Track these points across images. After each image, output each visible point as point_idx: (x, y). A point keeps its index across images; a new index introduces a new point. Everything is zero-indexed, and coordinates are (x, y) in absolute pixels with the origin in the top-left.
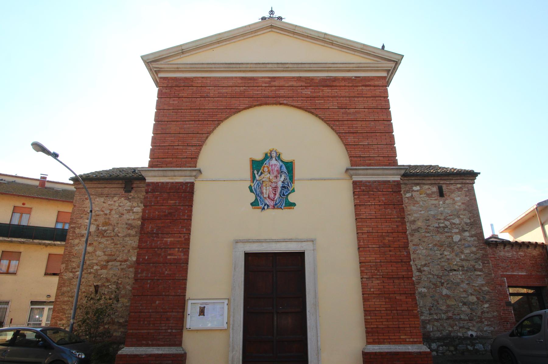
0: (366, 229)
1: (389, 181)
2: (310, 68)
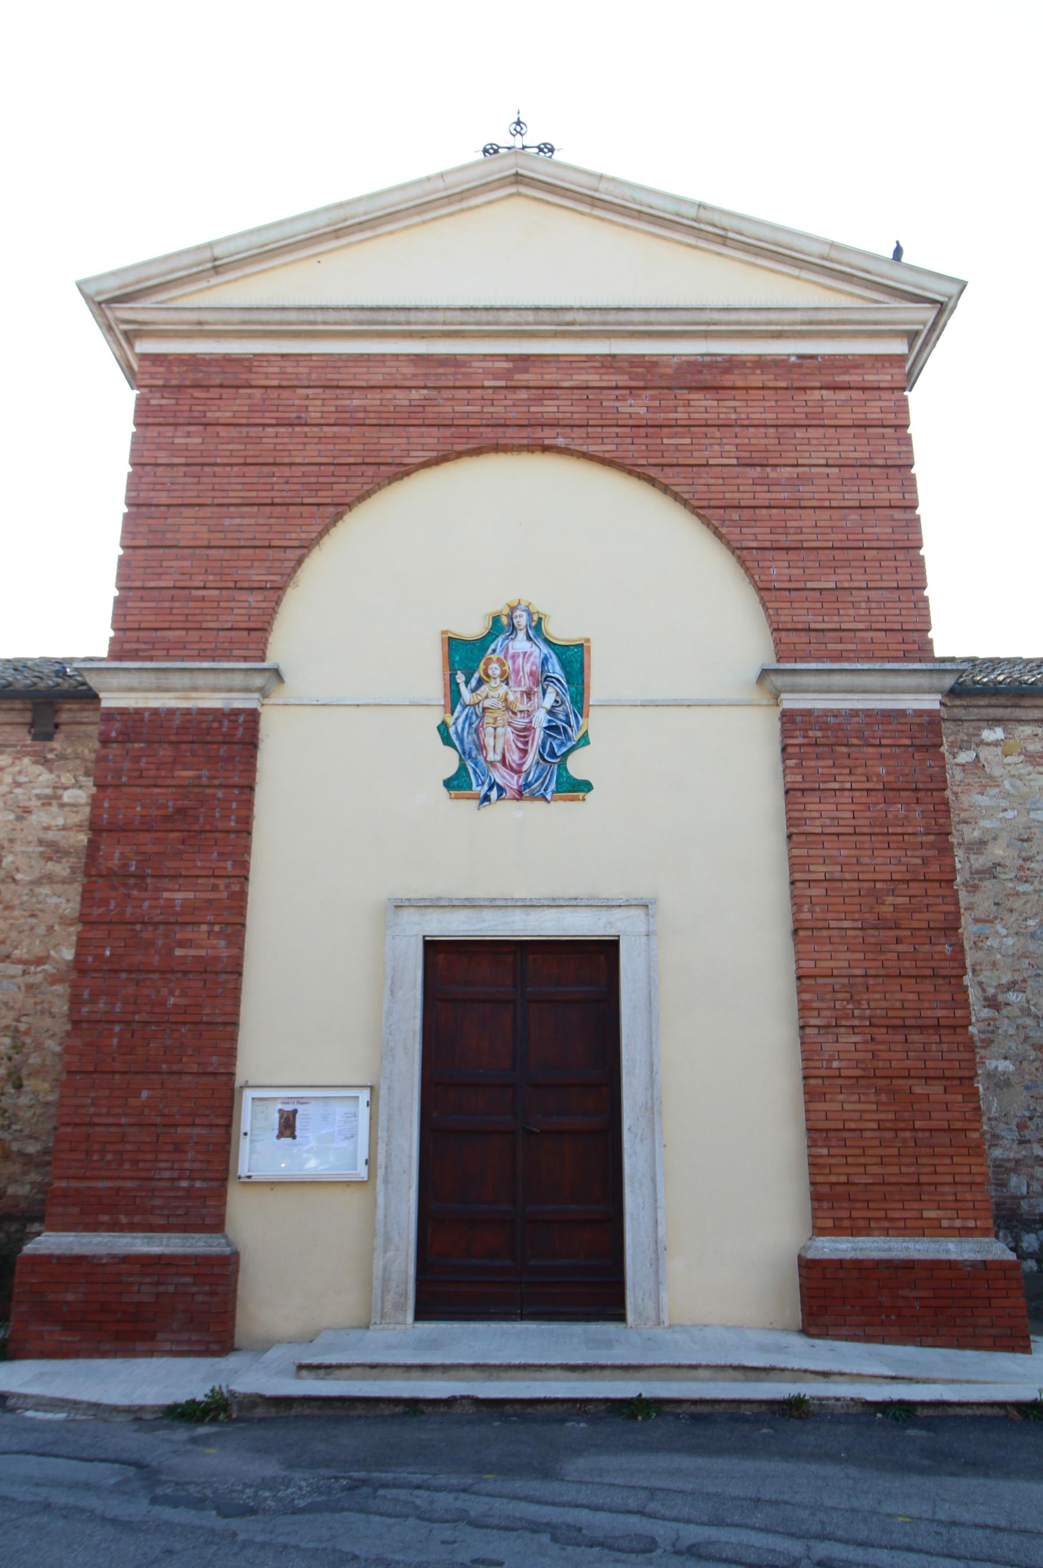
1: (902, 713)
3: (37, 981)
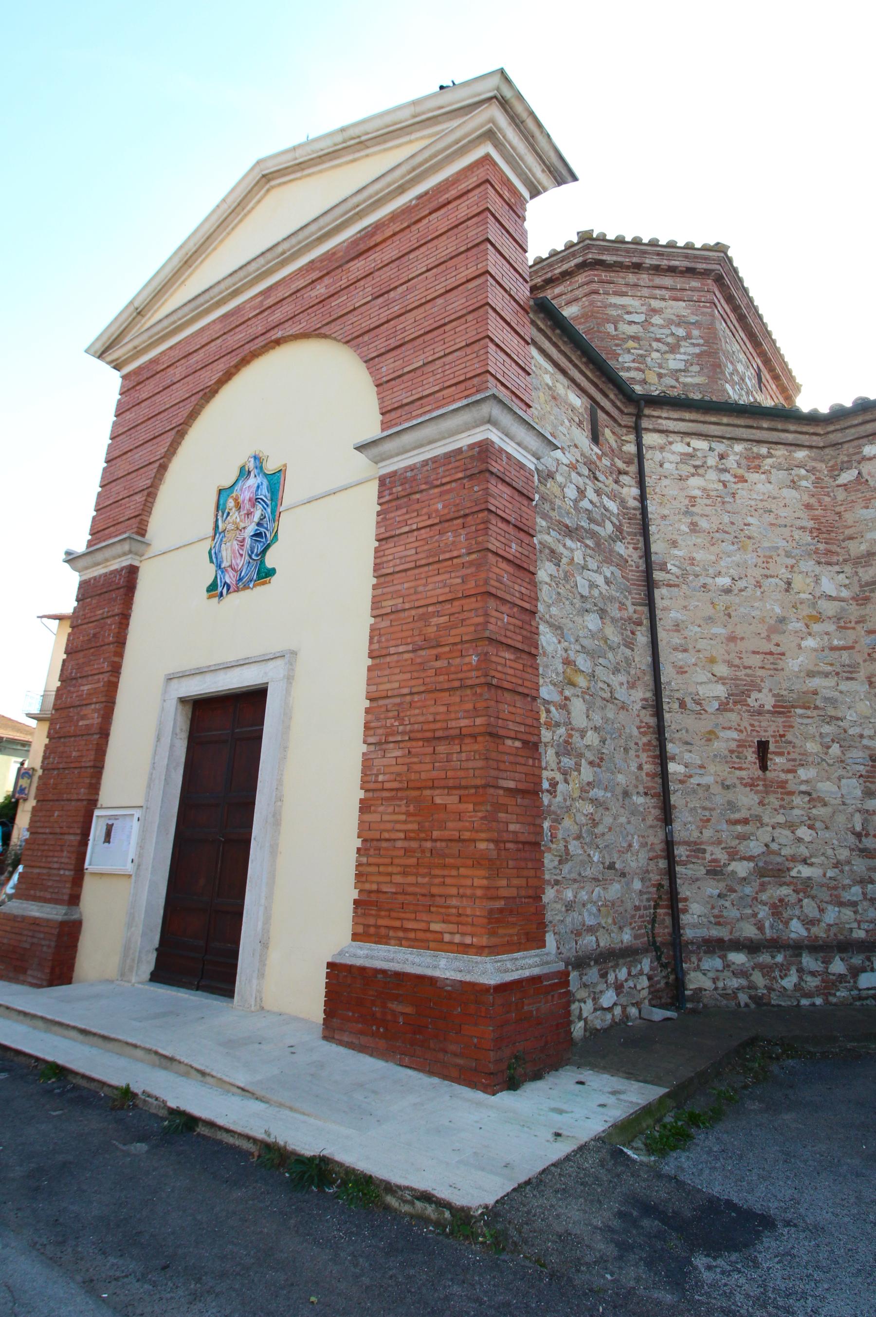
0: (390, 603)
1: (459, 451)
2: (320, 229)
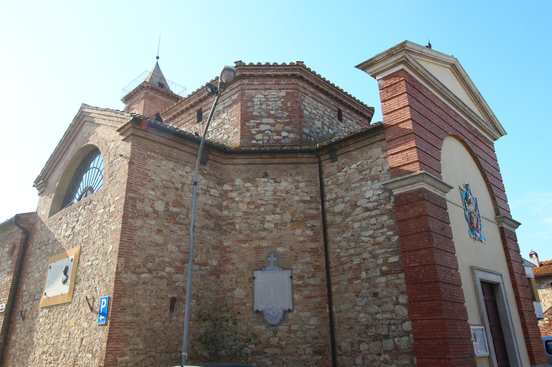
3: (204, 274)
